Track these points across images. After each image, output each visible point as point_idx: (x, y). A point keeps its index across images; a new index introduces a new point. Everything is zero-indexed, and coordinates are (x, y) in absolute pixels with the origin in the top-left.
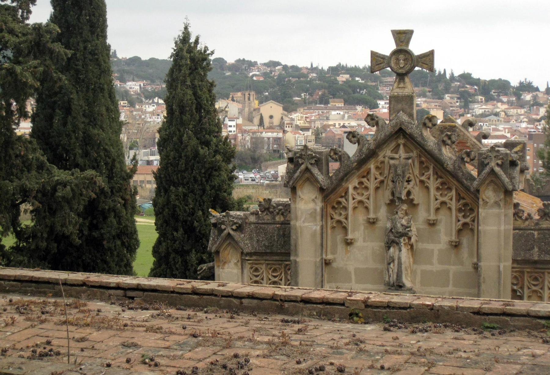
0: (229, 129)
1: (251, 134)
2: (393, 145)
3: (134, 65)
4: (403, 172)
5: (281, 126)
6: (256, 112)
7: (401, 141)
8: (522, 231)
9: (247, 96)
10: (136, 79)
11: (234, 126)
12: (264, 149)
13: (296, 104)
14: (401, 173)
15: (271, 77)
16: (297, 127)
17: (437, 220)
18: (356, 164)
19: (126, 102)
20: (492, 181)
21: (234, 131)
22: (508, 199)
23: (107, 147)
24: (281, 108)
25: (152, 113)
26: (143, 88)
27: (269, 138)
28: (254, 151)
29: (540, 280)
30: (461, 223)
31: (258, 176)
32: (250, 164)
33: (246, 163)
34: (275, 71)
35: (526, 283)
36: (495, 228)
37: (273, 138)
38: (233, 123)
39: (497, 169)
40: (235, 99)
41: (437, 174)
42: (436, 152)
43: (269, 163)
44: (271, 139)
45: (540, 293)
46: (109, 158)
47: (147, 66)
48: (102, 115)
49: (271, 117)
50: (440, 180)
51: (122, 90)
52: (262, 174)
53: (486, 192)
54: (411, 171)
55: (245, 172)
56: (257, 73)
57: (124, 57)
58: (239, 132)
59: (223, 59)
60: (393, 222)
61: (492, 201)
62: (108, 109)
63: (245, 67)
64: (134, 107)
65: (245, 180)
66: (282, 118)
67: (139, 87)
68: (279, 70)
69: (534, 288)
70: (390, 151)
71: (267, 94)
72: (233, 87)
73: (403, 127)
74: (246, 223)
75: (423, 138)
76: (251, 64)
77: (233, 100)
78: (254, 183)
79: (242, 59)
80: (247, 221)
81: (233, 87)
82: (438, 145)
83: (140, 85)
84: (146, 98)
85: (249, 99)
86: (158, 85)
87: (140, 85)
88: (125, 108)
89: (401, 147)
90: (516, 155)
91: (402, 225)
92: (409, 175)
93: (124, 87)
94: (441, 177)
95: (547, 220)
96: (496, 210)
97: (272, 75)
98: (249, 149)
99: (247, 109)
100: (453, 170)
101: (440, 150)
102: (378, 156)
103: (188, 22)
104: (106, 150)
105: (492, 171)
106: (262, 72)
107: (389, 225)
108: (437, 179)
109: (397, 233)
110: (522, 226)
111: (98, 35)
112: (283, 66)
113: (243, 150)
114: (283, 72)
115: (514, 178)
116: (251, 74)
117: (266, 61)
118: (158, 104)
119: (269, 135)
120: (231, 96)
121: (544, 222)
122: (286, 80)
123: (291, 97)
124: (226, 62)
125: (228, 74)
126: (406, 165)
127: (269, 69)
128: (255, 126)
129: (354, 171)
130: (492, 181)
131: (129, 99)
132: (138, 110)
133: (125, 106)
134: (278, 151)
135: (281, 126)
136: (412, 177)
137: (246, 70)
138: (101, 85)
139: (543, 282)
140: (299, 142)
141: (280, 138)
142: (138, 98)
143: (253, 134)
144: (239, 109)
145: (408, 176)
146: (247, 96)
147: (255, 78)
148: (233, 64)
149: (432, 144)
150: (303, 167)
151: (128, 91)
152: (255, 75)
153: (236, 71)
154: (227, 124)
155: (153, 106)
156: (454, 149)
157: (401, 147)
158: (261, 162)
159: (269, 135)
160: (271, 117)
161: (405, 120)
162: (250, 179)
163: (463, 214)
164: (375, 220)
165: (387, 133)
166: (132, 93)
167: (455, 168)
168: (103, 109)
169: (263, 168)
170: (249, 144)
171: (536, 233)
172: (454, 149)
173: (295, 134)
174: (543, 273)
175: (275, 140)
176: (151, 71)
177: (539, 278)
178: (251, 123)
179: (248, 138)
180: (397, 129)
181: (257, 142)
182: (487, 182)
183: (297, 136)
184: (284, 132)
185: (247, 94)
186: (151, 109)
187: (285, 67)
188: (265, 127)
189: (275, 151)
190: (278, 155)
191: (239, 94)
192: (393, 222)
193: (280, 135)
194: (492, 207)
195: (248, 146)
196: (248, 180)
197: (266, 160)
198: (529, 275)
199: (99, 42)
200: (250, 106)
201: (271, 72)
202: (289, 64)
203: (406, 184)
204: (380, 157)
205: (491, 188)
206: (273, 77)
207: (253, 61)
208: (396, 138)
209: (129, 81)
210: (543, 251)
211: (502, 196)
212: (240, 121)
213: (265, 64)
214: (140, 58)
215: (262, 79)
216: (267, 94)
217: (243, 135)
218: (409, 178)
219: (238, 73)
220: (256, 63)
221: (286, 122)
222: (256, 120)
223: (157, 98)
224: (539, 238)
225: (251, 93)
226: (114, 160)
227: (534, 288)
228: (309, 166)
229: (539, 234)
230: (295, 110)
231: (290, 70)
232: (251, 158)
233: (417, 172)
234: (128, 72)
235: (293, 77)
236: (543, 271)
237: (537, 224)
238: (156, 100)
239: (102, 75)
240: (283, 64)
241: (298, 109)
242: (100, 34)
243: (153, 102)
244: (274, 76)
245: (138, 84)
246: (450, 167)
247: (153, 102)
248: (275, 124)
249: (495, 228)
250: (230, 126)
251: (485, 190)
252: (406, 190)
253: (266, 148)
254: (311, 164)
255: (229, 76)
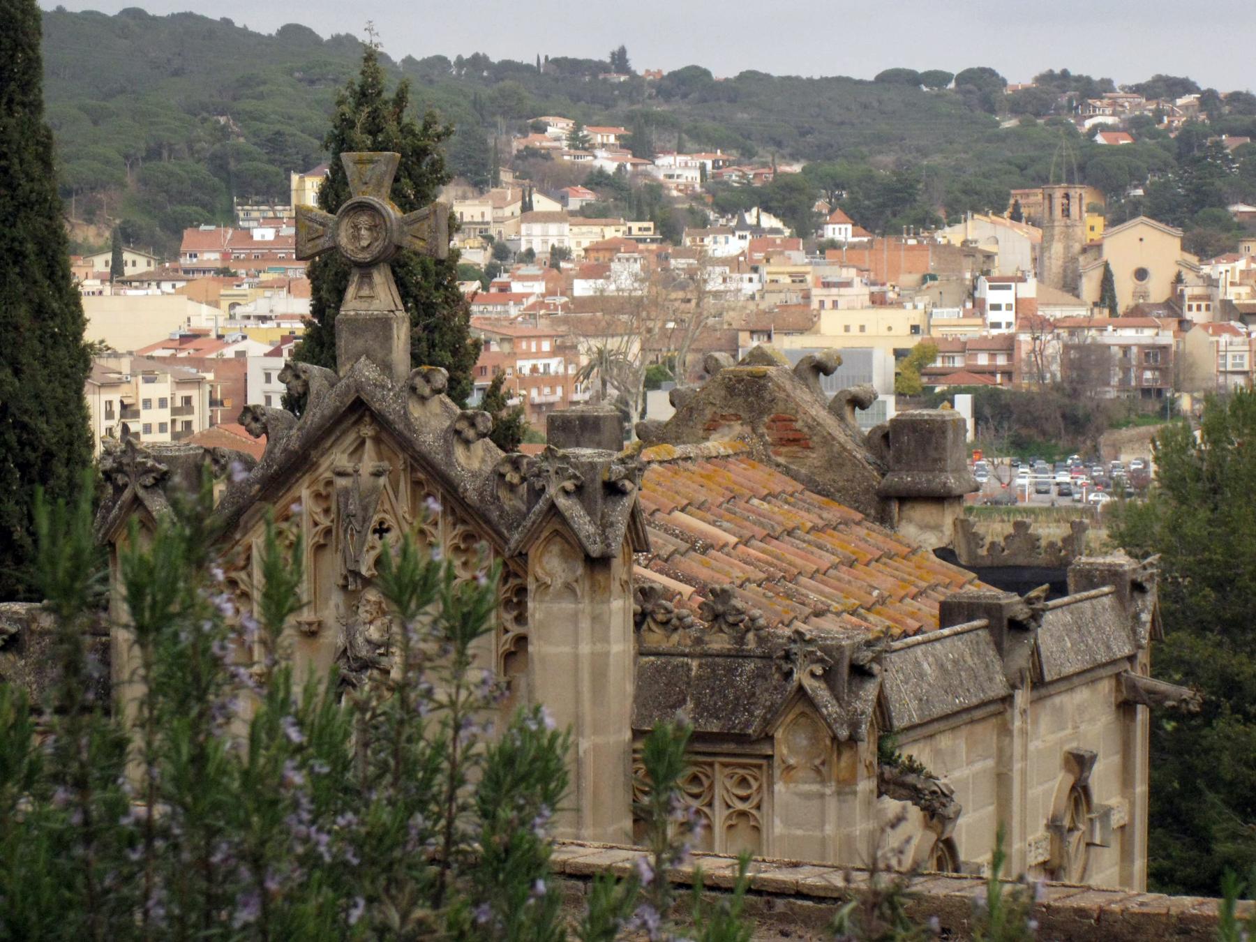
0: (992, 316)
1: (1064, 334)
2: (350, 439)
3: (685, 96)
4: (365, 509)
5: (1174, 305)
6: (1090, 255)
7: (367, 431)
8: (663, 659)
9: (1058, 201)
10: (689, 145)
11: (1009, 307)
12: (1108, 384)
13: (1241, 227)
14: (360, 514)
15: (1155, 135)
16: (1228, 308)
17: (320, 624)
18: (257, 487)
19: (651, 225)
20: (556, 532)
21: (1009, 325)
22: (600, 577)
23: (26, 419)
24: (1177, 243)
25: (733, 263)
26: (714, 176)
27: (1126, 349)
28: (1075, 394)
29: (706, 783)
30: (510, 635)
31: (1082, 480)
32: (1058, 436)
33: (1044, 433)
34: (1171, 113)
35: (718, 791)
36: (566, 649)
37: (1141, 347)
38: (1004, 297)
39: (562, 502)
40: (1024, 212)
41: (453, 512)
42: (439, 458)
43: (1125, 433)
44: (1135, 350)
45: (707, 816)
46: (35, 450)
47: (732, 101)
48: (16, 328)
49: (1141, 274)
50: (460, 528)
51: (641, 182)
52: (1098, 471)
53: (545, 559)
54: (387, 506)
55: (1040, 464)
56: (1110, 120)
57: (653, 69)
58: (1022, 328)
59: (991, 73)
60: (350, 631)
61: (559, 583)
62: (39, 311)
63: (1070, 101)
64: (678, 243)
65: (1038, 492)
66: (1179, 279)
67: (697, 174)
68: (1186, 107)
69: (740, 806)
70: (345, 456)
71: (1140, 192)
72: (1022, 169)
73: (364, 397)
74: (32, 632)
75: (408, 424)
76: (1091, 90)
77: (1016, 217)
78: (1065, 502)
79: (1057, 71)
80: (34, 626)
81: (1022, 169)
82: (446, 441)
83: (703, 168)
84: (723, 209)
85: (1066, 212)
86: (764, 165)
87: (703, 168)
88: (641, 246)
89: (369, 444)
90: (621, 468)
91: (369, 642)
92: (382, 515)
93: (646, 175)
94: (464, 522)
95: (721, 631)
96: (567, 606)
97: (1161, 127)
98: (1057, 387)
99: (1057, 248)
100: (478, 504)
101: (449, 453)
102: (314, 466)
103: (375, 40)
104: (24, 427)
105: (553, 507)
106: (1128, 115)
107: (341, 641)
108: (454, 525)
109: (356, 659)
110: (664, 646)
111: (10, 101)
112: (1203, 93)
113: (1034, 389)
114: (1202, 117)
115: (612, 525)
116: (1088, 124)
117: (1144, 78)
118: (757, 229)
119: (1128, 335)
120: (1012, 201)
121: (714, 637)
122: (1208, 142)
123: (1223, 204)
124: (1004, 82)
125: (1010, 123)
126: (375, 489)
127: (1153, 107)
128: (1083, 304)
129: (257, 505)
130: (556, 532)
131: (657, 211)
132: (688, 253)
133: (643, 241)
134: (1159, 392)
135: (1174, 305)
136: (390, 520)
137: (1071, 108)
138: (16, 244)
139: (711, 787)
140: (1230, 361)
141: (1165, 348)
142: (691, 211)
143: (1072, 334)
144: (1033, 248)
145: (376, 518)
146: (1058, 201)
147: (1100, 139)
148: (1027, 90)
149: (430, 438)
150: (127, 494)
151: (661, 186)
152: (1103, 128)
153: (1038, 115)
154: (983, 301)
155: (742, 237)
156: (762, 436)
157: (369, 444)
158: (1099, 431)
159: (1128, 335)
160: (1141, 274)
161: (368, 378)
162: (1054, 490)
163: (515, 613)
164: (314, 628)
165: (326, 412)
166: (675, 193)
167: (482, 500)
168: (22, 313)
169: (1104, 451)
170: (1055, 368)
171: (694, 664)
172: (762, 436)
173: (1219, 330)
174: (711, 765)
175: (1147, 355)
176: (742, 116)
177: (703, 778)
178: (1069, 297)
179: (1053, 347)
180: (349, 401)
181: (1085, 362)
182: (545, 534)
183: (1225, 338)
184: (1184, 325)
185: (1058, 194)
186: (733, 246)
187: (1209, 99)
188: (1121, 309)
189: (1146, 392)
190: (1158, 407)
191: (1037, 196)
192: (350, 631)
193: (1167, 337)
194: (558, 597)
195: (1053, 375)
196: (1047, 492)
197: (1115, 425)
198: (728, 771)
199: (13, 121)
200: (1067, 237)
201: (1159, 115)
202: (1223, 89)
203: (372, 538)
204: (321, 470)
205: (555, 549)
206: (1163, 134)
207: (1096, 77)
208: (356, 423)
209: (667, 152)
210: (706, 709)
211: (580, 571)
212: (1029, 289)
213: (1138, 89)
214: (706, 73)
215: (1124, 141)
216: (1140, 192)
217: (1035, 339)
218: (381, 523)
219: (1040, 121)
220: (1107, 85)
221: (1188, 292)
222: (1090, 287)
223: (754, 211)
224: (699, 678)
225: (1072, 192)
226: (49, 455)
227: (740, 806)
228: (141, 493)
229: (700, 666)
230: (1229, 250)
231: (1226, 109)
232: (1064, 416)
233: (404, 507)
234: (665, 123)
235: (1233, 133)
236: (709, 759)
237: (698, 641)
238: (751, 218)
239: (22, 214)
240: (1203, 87)
241: (1242, 246)
242: (18, 97)
243: (742, 225)
244: (1169, 128)
245: (694, 161)
246: (472, 497)
247: (742, 225)
248: (1152, 300)
249: (566, 649)
250: (996, 307)
251: (542, 555)
252: (373, 554)
253: (1115, 381)
254: (145, 487)
255: (1009, 133)
